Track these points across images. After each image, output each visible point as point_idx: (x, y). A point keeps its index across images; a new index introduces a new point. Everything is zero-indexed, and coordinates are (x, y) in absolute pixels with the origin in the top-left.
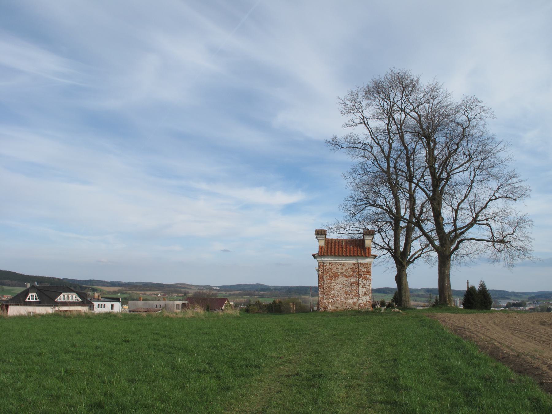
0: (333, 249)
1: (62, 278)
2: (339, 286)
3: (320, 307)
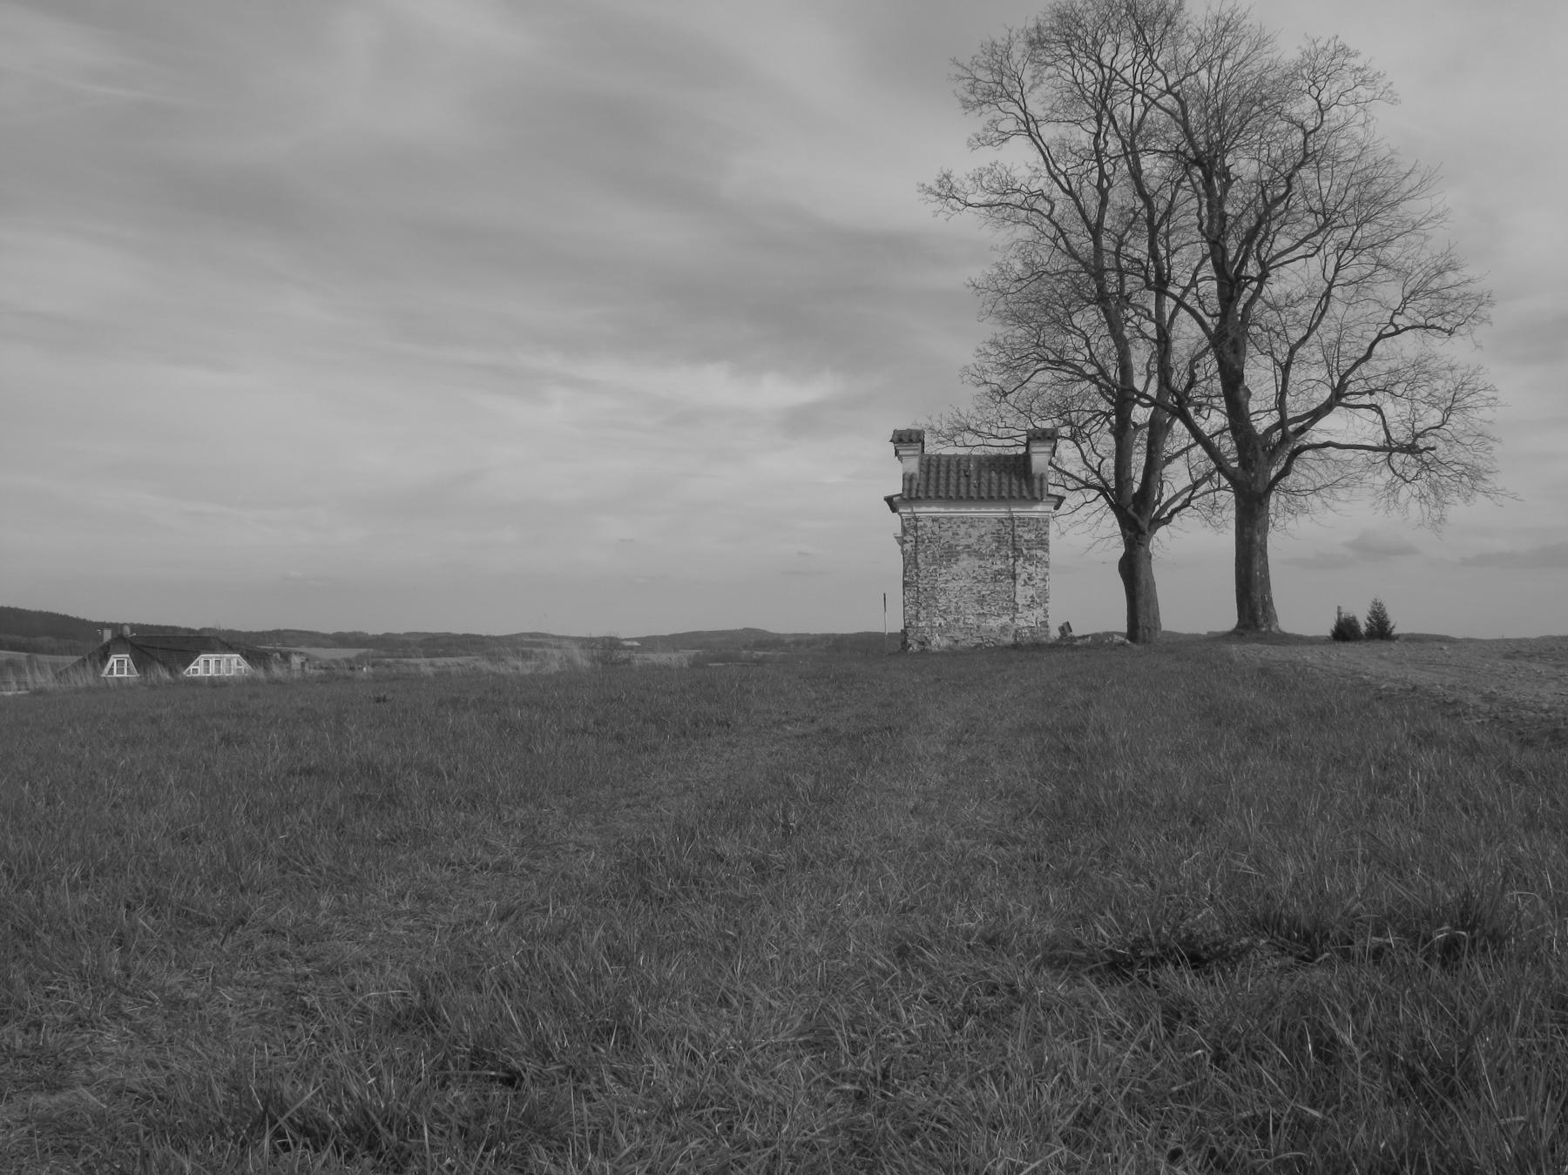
0: (942, 481)
1: (198, 629)
2: (962, 583)
3: (909, 641)
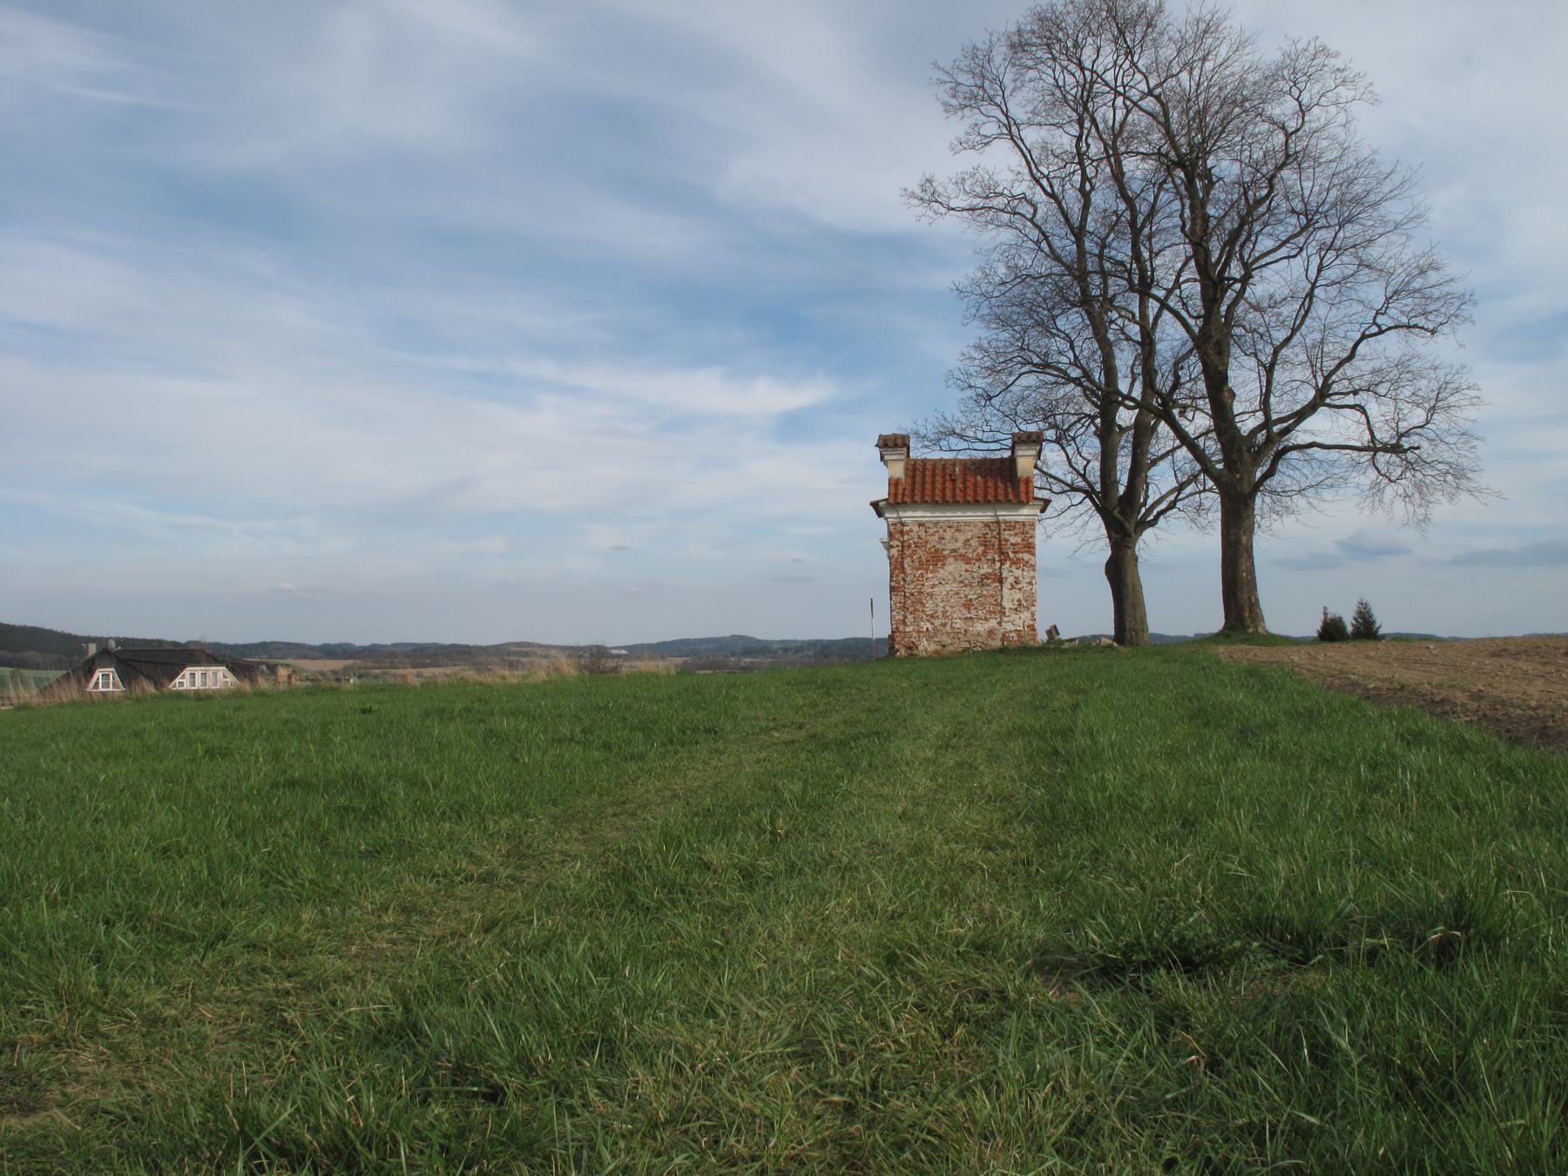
0: (928, 486)
2: (948, 588)
3: (897, 646)
